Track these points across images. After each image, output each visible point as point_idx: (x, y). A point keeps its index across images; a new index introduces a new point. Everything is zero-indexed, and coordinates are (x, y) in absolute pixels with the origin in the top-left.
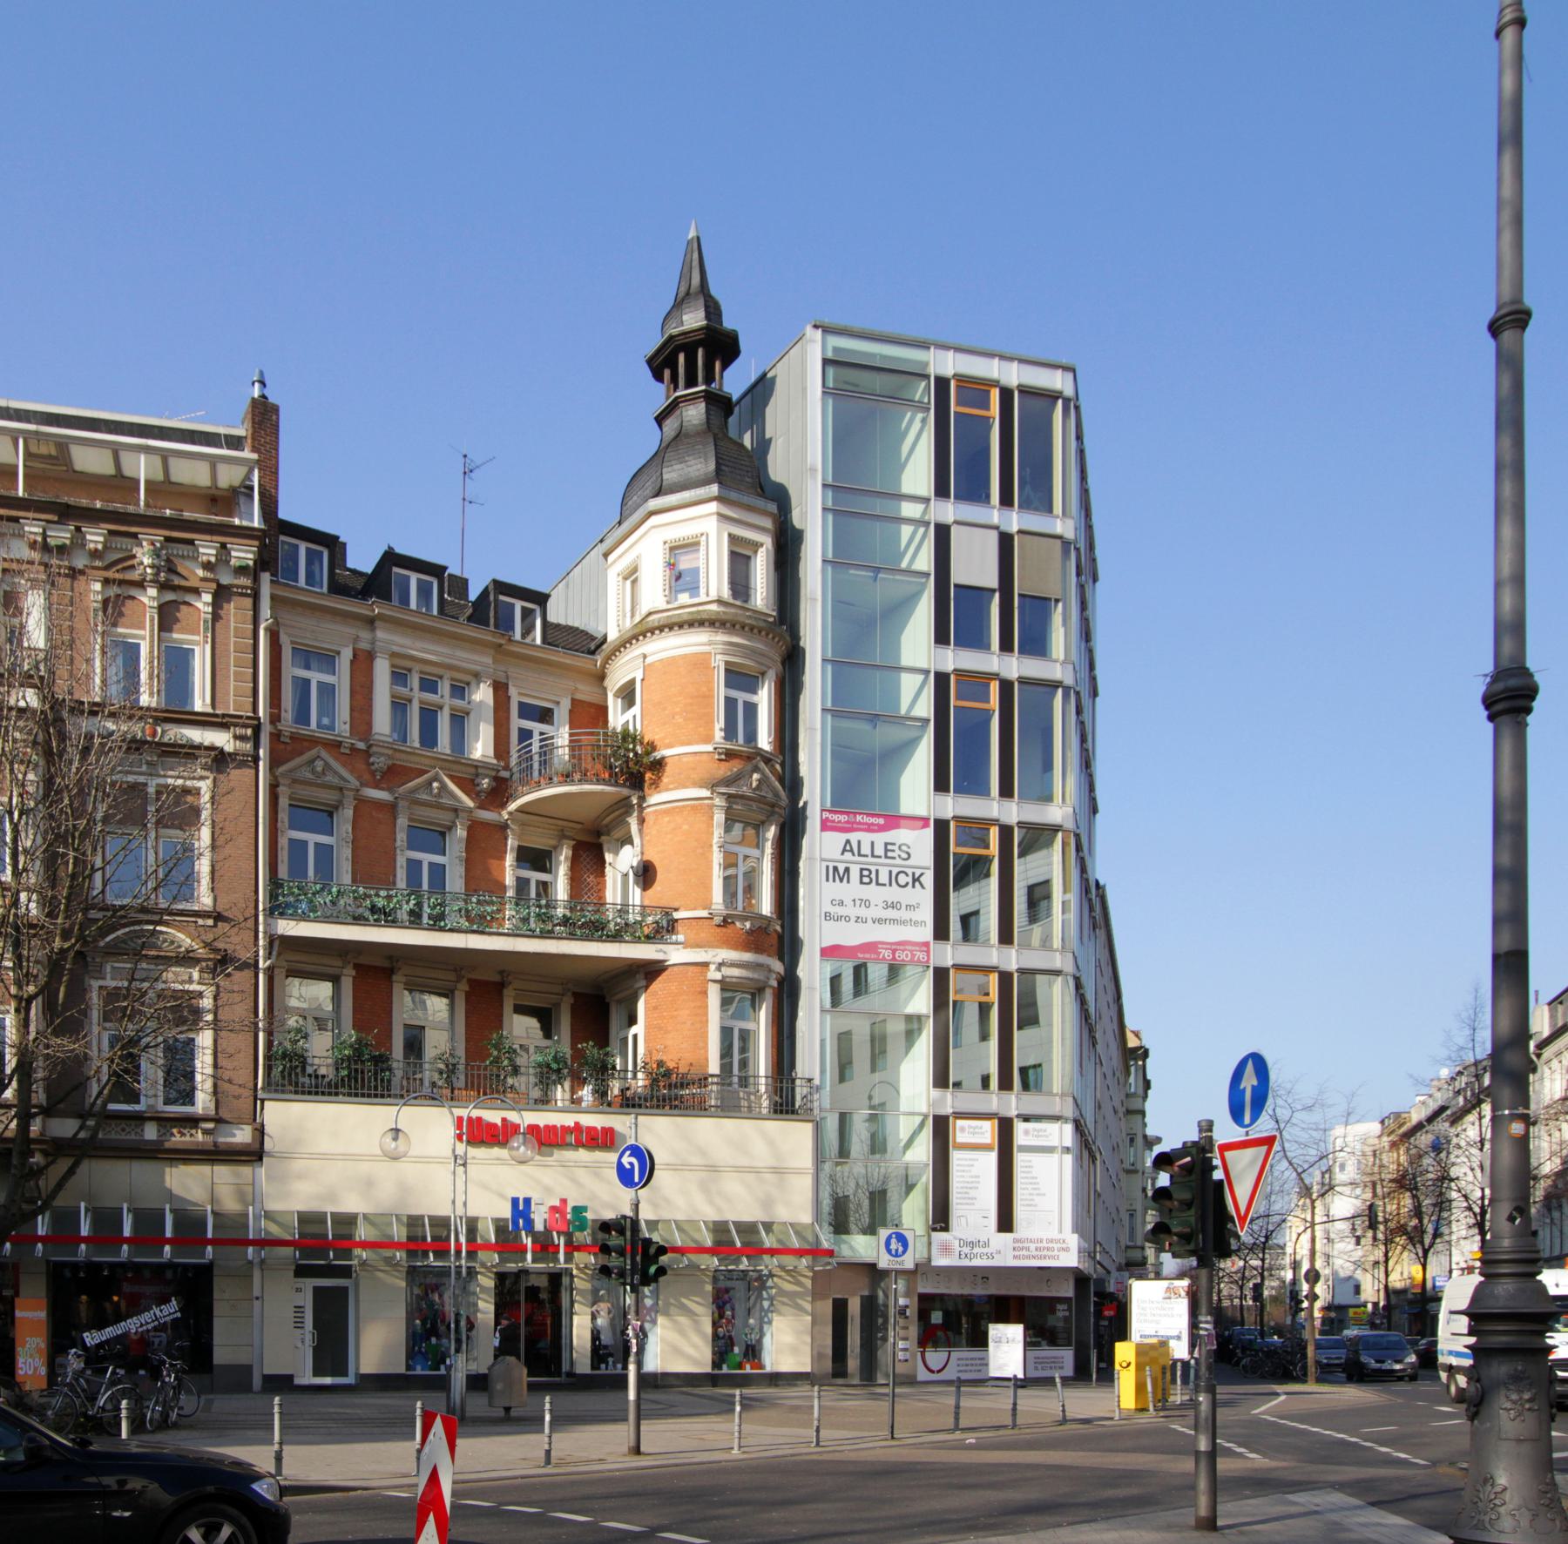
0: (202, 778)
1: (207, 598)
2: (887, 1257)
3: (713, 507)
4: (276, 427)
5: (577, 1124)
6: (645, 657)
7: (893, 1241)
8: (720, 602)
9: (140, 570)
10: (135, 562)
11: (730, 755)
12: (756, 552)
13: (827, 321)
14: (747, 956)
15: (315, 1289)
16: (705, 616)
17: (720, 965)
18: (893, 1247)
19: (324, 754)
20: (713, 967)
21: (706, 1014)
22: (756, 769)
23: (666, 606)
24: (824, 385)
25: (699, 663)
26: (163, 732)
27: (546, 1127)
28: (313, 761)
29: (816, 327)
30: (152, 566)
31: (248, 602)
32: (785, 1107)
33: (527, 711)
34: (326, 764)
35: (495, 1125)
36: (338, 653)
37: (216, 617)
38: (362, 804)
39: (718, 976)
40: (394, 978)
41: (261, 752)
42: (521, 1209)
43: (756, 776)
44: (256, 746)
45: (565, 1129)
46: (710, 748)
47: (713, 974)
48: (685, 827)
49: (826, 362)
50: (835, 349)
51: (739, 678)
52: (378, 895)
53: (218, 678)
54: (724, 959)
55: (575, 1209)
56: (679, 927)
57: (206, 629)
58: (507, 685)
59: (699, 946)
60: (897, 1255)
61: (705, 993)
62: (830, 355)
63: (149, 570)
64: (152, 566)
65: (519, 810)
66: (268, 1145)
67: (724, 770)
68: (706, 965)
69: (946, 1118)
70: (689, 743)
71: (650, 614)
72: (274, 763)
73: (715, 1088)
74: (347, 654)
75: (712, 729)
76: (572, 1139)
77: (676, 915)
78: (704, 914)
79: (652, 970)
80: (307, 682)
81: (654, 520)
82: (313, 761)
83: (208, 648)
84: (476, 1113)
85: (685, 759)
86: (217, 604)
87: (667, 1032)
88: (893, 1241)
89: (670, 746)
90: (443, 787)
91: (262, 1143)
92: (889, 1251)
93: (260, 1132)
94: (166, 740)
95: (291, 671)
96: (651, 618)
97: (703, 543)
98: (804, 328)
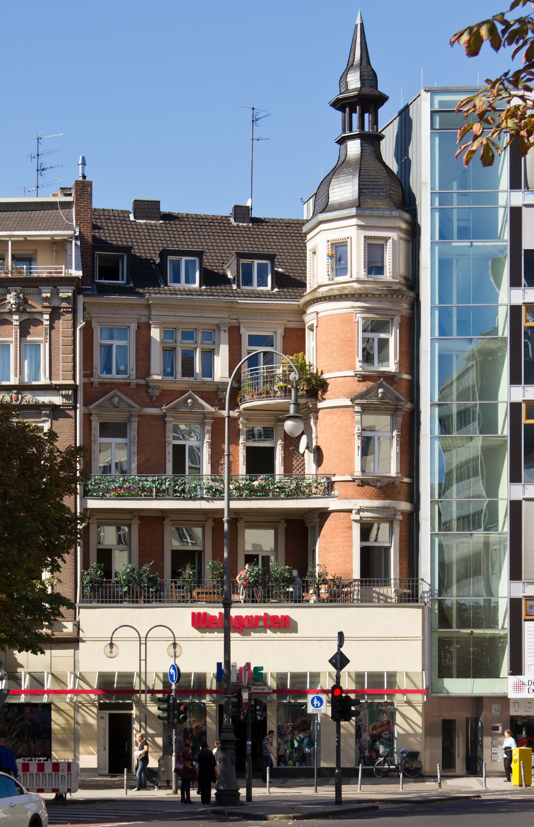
0: (44, 421)
1: (47, 317)
2: (312, 708)
3: (354, 221)
4: (90, 195)
5: (266, 614)
6: (318, 313)
7: (315, 700)
8: (358, 281)
9: (9, 306)
10: (6, 302)
11: (364, 378)
12: (387, 242)
13: (435, 85)
14: (377, 503)
15: (110, 714)
16: (346, 292)
17: (359, 511)
18: (315, 702)
19: (118, 393)
20: (354, 512)
21: (351, 541)
22: (380, 386)
23: (327, 282)
24: (432, 128)
25: (346, 319)
26: (22, 398)
27: (247, 617)
28: (112, 398)
29: (427, 91)
30: (16, 304)
31: (70, 316)
32: (409, 596)
33: (254, 340)
34: (120, 398)
35: (215, 617)
36: (129, 327)
37: (51, 327)
38: (141, 416)
39: (357, 517)
40: (165, 523)
41: (78, 405)
42: (248, 665)
43: (380, 390)
44: (75, 402)
45: (258, 618)
46: (353, 374)
47: (355, 516)
48: (338, 423)
49: (433, 113)
50: (440, 102)
51: (375, 326)
52: (147, 481)
53: (53, 361)
54: (364, 503)
55: (255, 668)
56: (336, 486)
57: (46, 334)
58: (239, 327)
59: (346, 498)
60: (317, 707)
61: (351, 527)
62: (436, 108)
63: (14, 306)
64: (16, 304)
65: (245, 409)
66: (81, 635)
67: (362, 387)
68: (350, 511)
69: (520, 600)
70: (341, 370)
71: (320, 286)
72: (86, 404)
73: (356, 588)
74: (134, 327)
75: (354, 361)
76: (261, 623)
77: (334, 479)
78: (349, 478)
79: (323, 515)
80: (110, 347)
81: (322, 227)
82: (112, 398)
83: (47, 345)
84: (202, 610)
85: (339, 380)
86: (52, 320)
87: (330, 552)
88: (315, 700)
89: (331, 371)
90: (195, 401)
91: (78, 633)
92: (313, 705)
93: (77, 626)
94: (24, 403)
95: (99, 340)
96: (321, 290)
97: (349, 244)
98: (420, 91)
